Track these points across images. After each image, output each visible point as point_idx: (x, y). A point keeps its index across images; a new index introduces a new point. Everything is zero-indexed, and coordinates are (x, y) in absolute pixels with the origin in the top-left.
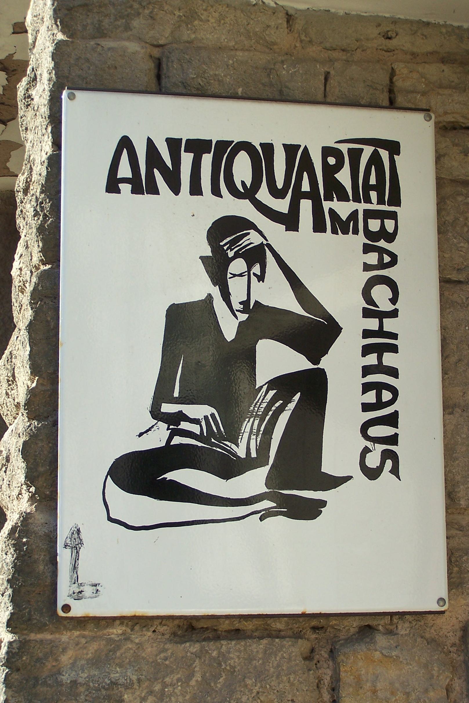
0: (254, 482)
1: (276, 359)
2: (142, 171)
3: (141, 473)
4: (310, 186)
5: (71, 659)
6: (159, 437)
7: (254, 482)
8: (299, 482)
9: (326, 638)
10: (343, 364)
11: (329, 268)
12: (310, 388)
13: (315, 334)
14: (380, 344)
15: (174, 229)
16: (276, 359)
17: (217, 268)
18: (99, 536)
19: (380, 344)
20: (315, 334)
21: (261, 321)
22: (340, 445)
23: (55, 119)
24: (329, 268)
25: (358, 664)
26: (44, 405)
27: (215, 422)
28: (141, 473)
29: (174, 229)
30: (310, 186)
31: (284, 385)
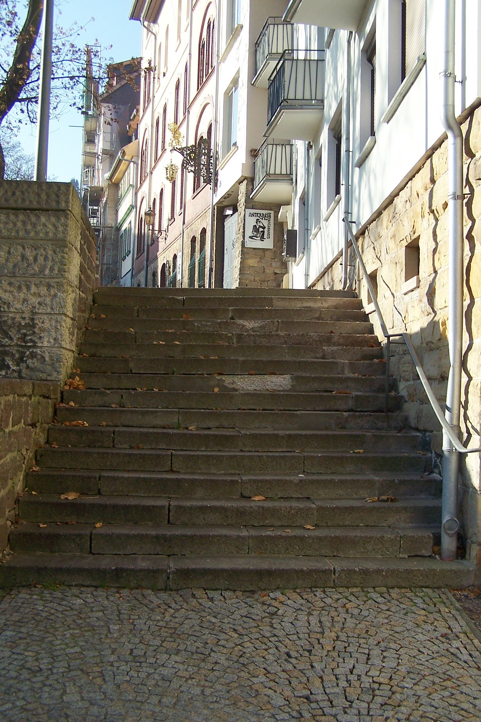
0: (259, 238)
1: (261, 229)
2: (252, 215)
3: (251, 237)
4: (264, 216)
5: (245, 250)
6: (252, 235)
7: (259, 238)
8: (262, 238)
9: (264, 250)
10: (266, 230)
11: (265, 223)
12: (264, 232)
13: (264, 228)
14: (269, 229)
15: (254, 219)
16: (261, 229)
17: (257, 222)
18: (248, 241)
19: (269, 229)
20: (264, 228)
21: (260, 227)
22: (265, 236)
23: (231, 40)
24: (265, 223)
25: (266, 252)
26: (244, 232)
27: (202, 240)
28: (251, 237)
29: (254, 219)
30: (264, 216)
31: (261, 231)
